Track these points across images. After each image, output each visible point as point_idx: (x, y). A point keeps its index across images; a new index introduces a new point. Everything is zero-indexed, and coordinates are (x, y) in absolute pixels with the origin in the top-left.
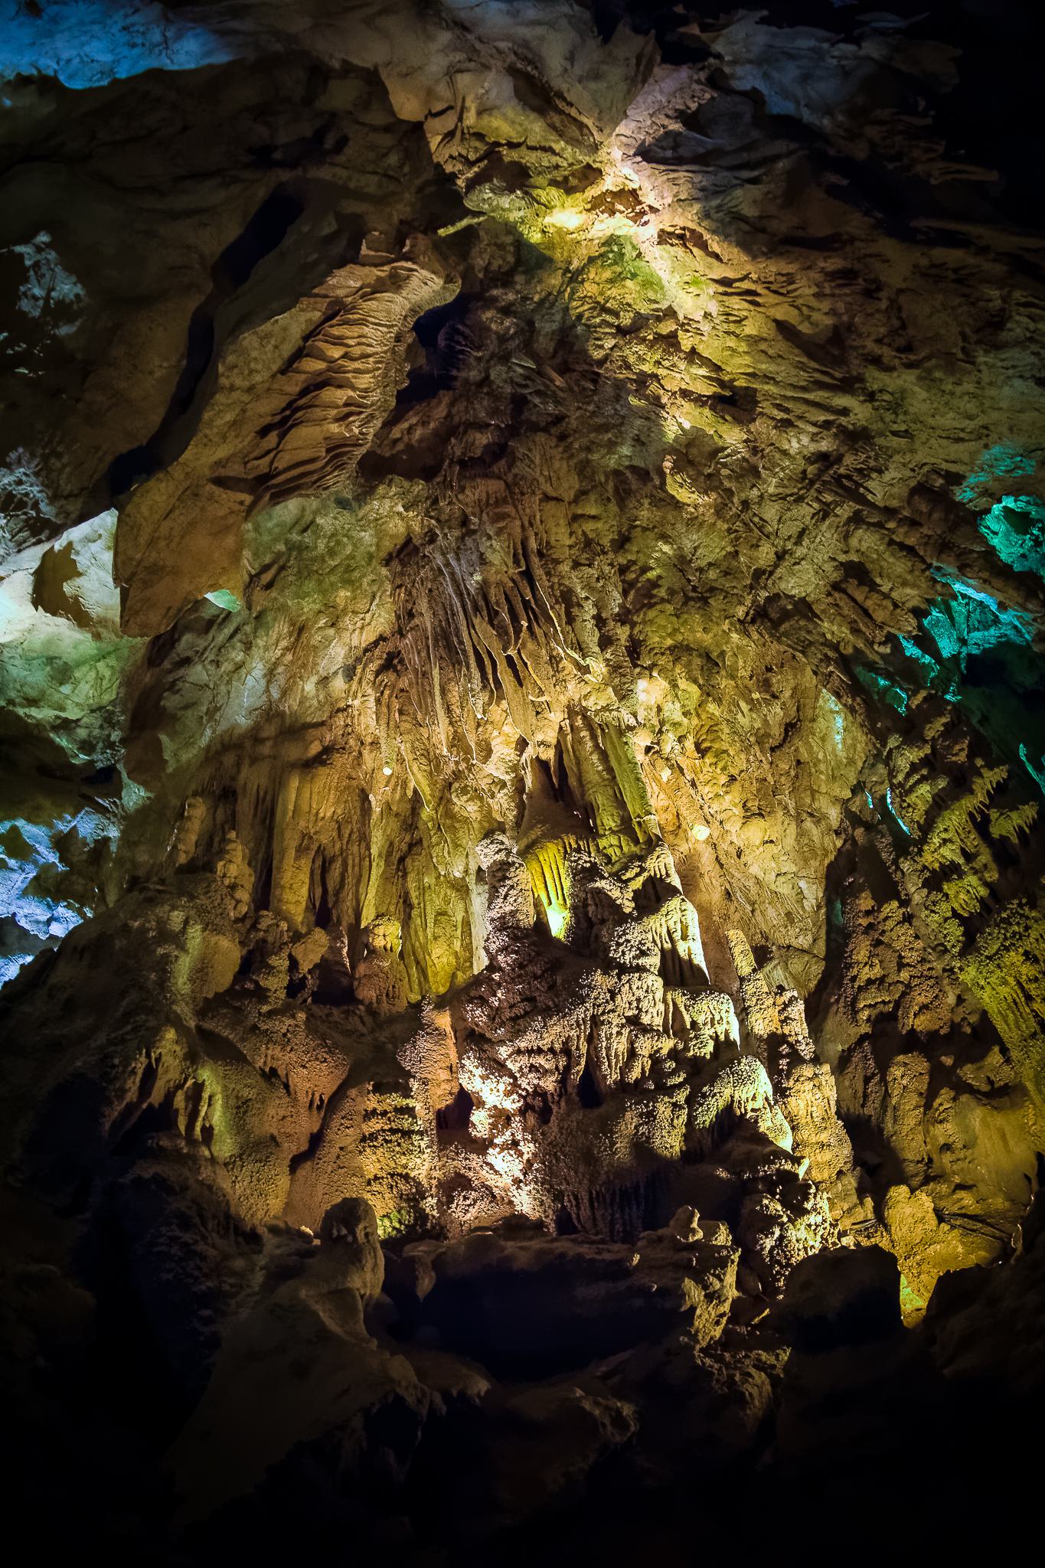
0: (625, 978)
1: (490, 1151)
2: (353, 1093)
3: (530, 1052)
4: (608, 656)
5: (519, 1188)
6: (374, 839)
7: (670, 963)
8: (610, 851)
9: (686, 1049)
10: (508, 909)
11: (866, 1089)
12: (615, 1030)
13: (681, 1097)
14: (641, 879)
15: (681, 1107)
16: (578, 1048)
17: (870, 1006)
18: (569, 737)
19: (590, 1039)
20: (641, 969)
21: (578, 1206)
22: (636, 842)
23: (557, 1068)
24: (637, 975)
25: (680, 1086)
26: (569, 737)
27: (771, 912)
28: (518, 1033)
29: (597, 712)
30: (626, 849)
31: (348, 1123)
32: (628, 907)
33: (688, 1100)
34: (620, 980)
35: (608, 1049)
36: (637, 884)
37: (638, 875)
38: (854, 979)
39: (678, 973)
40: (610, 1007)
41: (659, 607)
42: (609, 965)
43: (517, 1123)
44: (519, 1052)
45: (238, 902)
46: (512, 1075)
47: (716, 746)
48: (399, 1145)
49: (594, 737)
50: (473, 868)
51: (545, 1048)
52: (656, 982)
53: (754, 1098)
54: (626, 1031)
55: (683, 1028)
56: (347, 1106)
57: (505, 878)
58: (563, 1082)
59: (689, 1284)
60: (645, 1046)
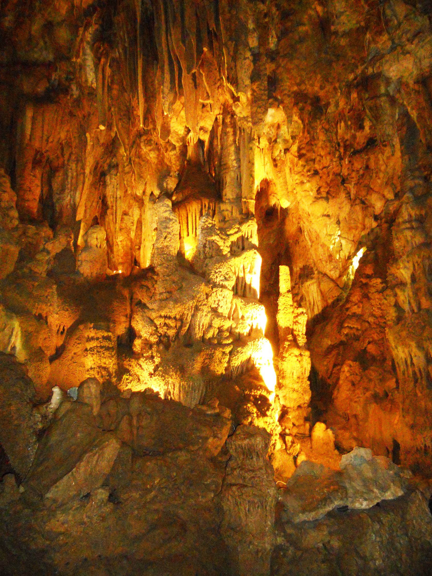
0: (215, 290)
1: (142, 359)
2: (81, 327)
3: (165, 317)
4: (254, 87)
5: (151, 377)
6: (88, 164)
7: (240, 285)
8: (226, 213)
9: (236, 328)
10: (165, 244)
11: (333, 370)
12: (205, 313)
13: (228, 350)
15: (226, 355)
16: (186, 319)
17: (350, 328)
18: (220, 128)
19: (193, 316)
20: (223, 287)
21: (174, 389)
23: (176, 326)
24: (220, 289)
25: (228, 345)
26: (220, 128)
27: (321, 250)
28: (161, 308)
29: (241, 119)
30: (234, 214)
31: (78, 341)
32: (226, 251)
33: (231, 353)
34: (212, 289)
35: (200, 322)
36: (234, 238)
38: (347, 309)
39: (241, 290)
40: (204, 303)
42: (208, 282)
43: (155, 348)
44: (161, 317)
46: (156, 326)
47: (309, 155)
48: (104, 353)
49: (235, 134)
50: (148, 192)
51: (173, 317)
52: (229, 294)
53: (261, 358)
54: (209, 315)
55: (238, 318)
56: (78, 333)
57: (166, 227)
58: (178, 334)
60: (217, 323)
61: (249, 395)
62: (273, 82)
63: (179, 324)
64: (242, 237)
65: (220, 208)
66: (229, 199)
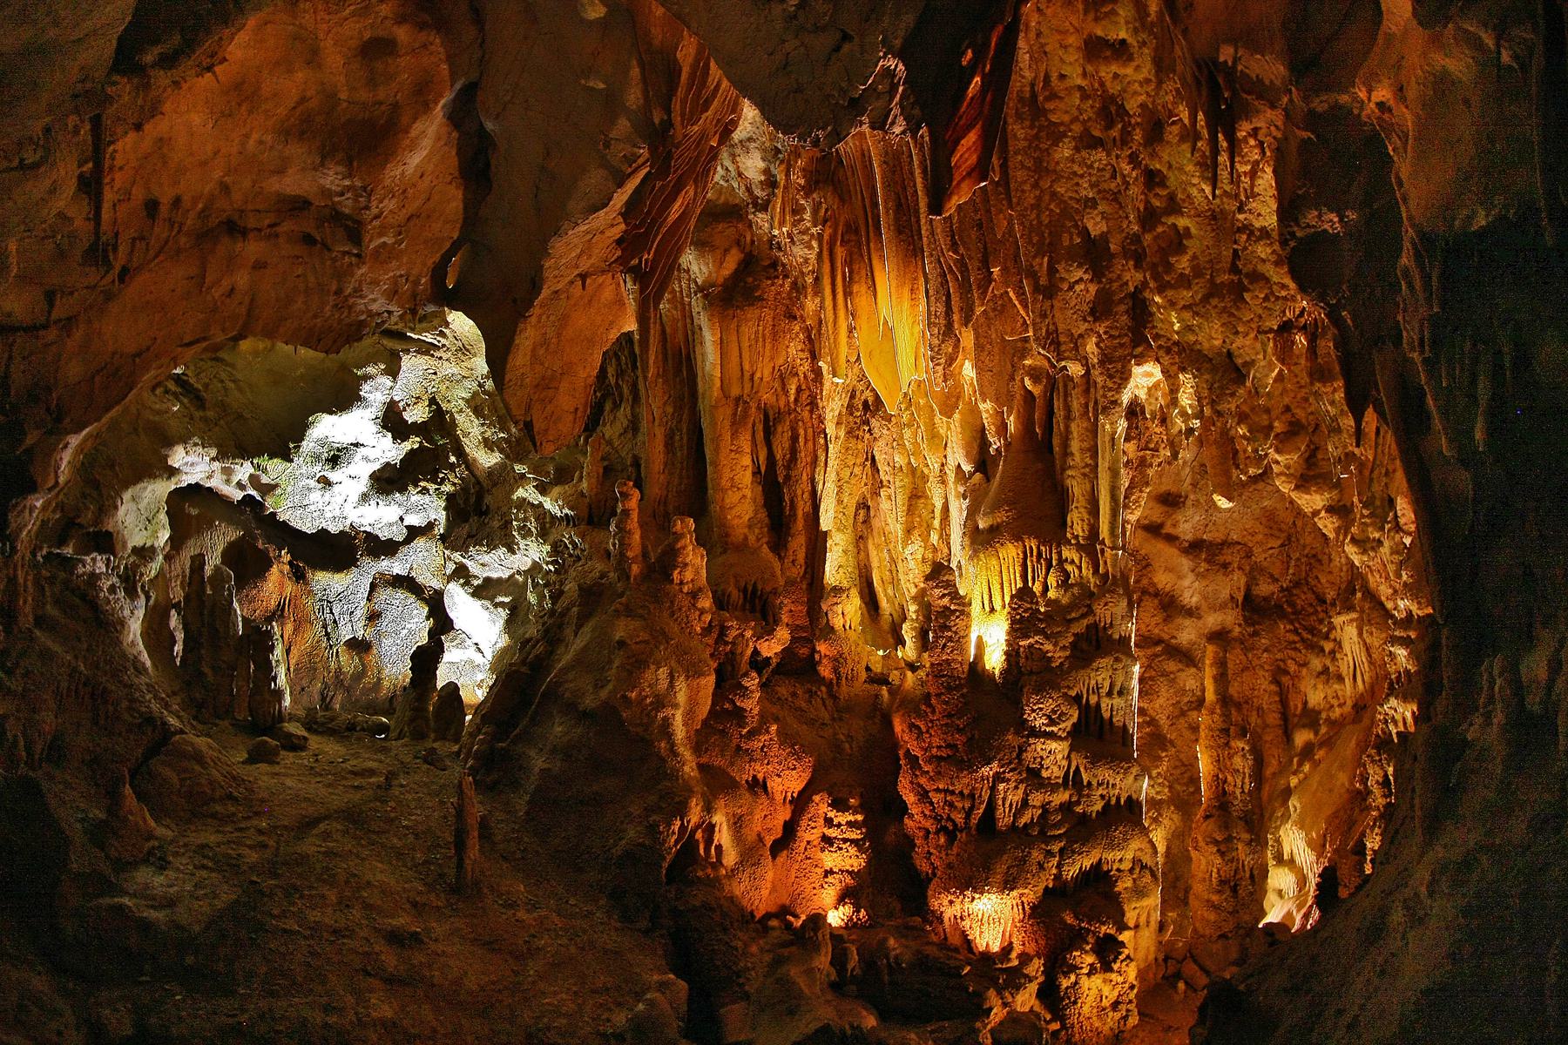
3: (946, 791)
8: (1069, 568)
13: (1056, 848)
14: (1085, 622)
22: (1096, 571)
33: (1061, 851)
35: (1004, 799)
37: (1083, 616)
41: (1170, 293)
45: (702, 612)
54: (1022, 787)
59: (992, 993)
60: (1037, 799)
61: (1088, 931)
62: (1140, 313)
63: (967, 805)
64: (1095, 625)
65: (1060, 554)
66: (1076, 537)
